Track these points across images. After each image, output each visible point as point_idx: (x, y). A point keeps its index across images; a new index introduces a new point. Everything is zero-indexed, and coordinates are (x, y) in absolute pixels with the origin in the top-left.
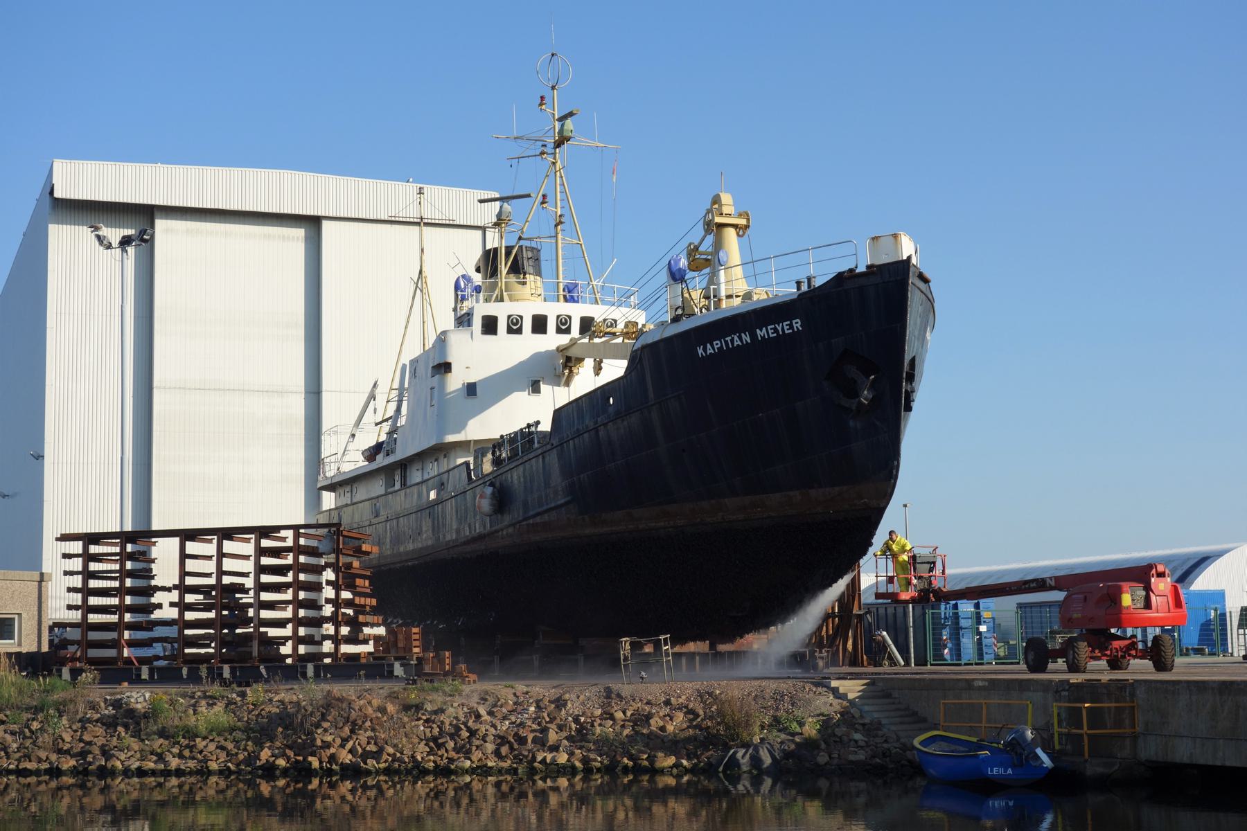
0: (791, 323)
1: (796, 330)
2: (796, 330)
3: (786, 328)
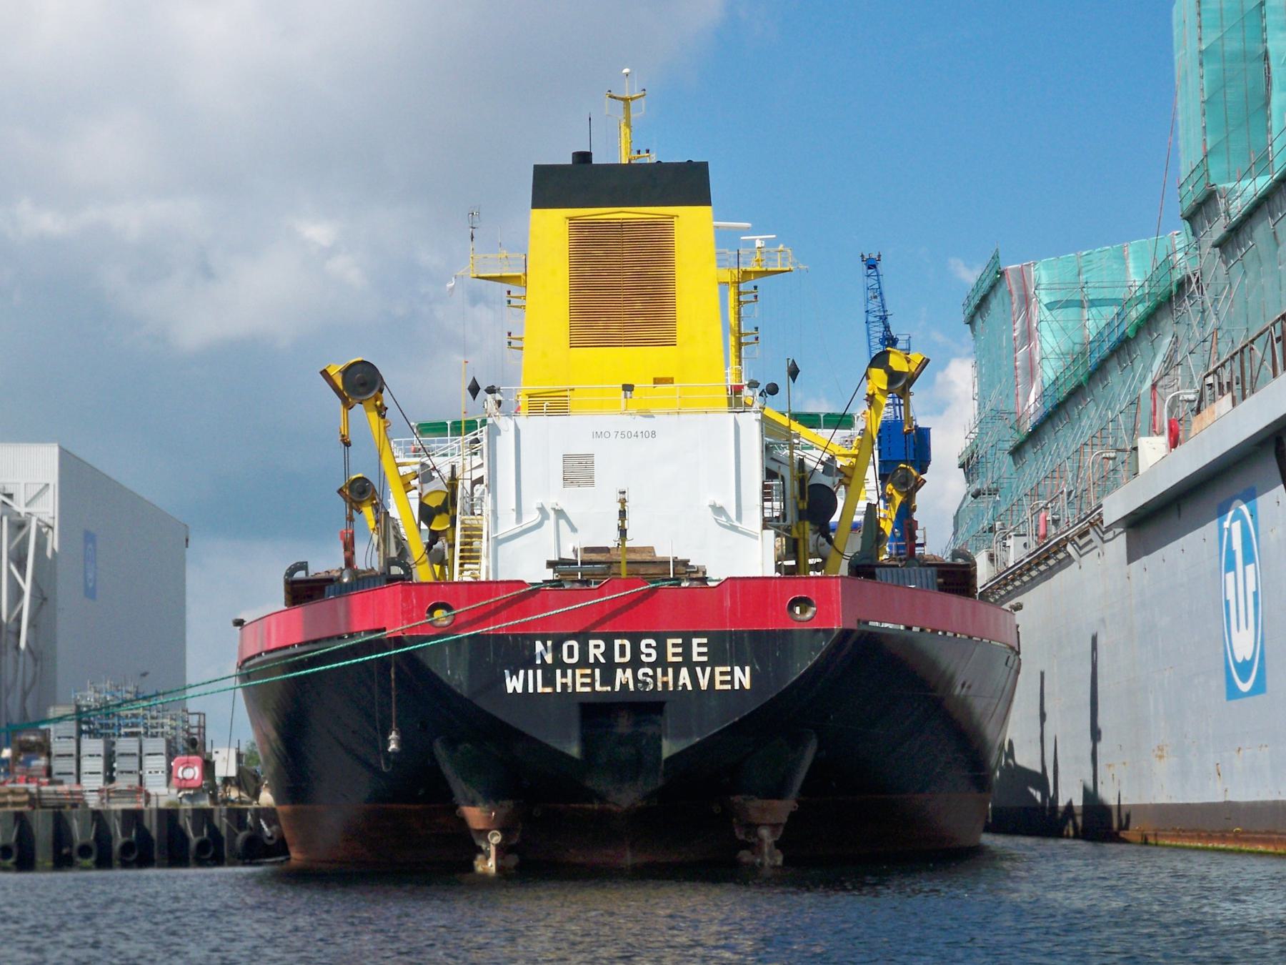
0: (731, 673)
1: (737, 687)
2: (737, 687)
3: (718, 678)
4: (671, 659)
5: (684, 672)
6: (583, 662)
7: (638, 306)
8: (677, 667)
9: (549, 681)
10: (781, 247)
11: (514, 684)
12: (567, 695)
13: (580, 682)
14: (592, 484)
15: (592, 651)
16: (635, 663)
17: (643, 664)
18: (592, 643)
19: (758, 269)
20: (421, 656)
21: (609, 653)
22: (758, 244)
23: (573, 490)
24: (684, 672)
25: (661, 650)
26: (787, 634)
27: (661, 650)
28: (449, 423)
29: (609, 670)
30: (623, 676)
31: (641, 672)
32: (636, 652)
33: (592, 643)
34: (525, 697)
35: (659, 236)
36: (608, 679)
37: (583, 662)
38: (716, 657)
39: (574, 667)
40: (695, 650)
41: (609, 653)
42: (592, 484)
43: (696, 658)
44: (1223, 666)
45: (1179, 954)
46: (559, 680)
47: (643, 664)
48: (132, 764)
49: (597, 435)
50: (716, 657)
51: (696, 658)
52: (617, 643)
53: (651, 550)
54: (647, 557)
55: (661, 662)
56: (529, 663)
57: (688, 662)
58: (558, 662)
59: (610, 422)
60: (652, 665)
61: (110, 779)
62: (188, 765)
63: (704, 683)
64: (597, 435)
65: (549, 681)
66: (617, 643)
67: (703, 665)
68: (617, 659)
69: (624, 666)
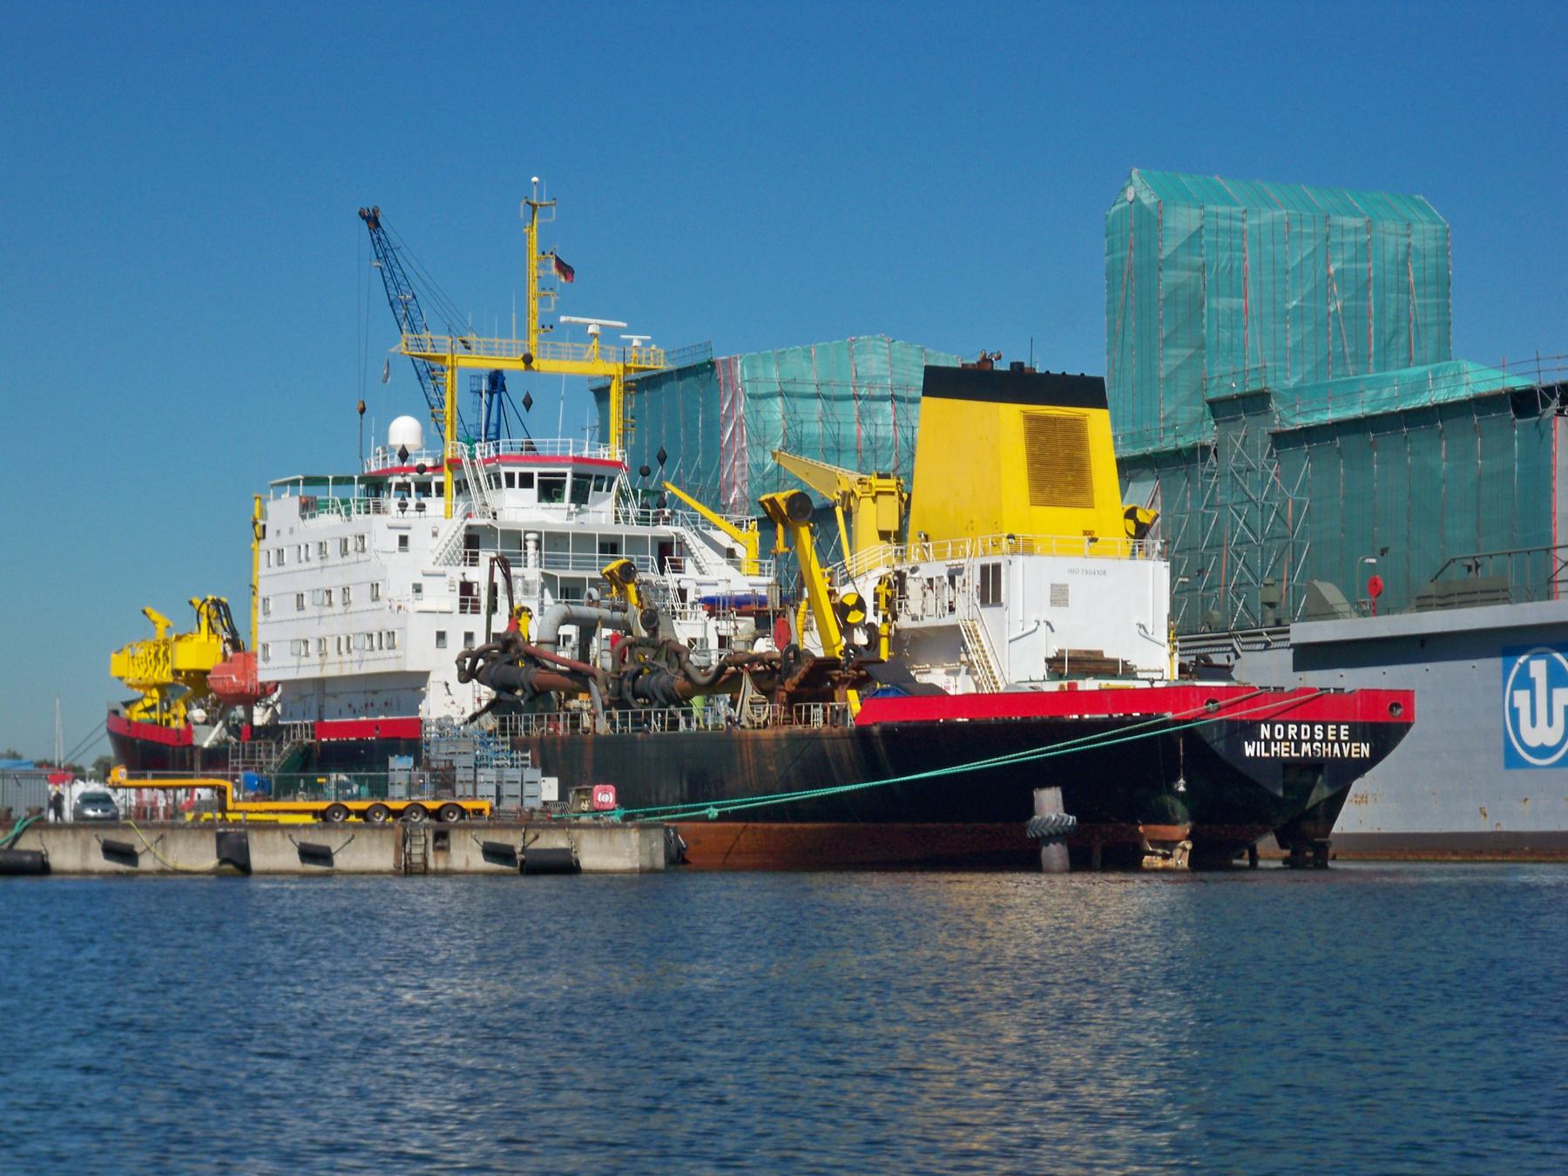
3: (1353, 750)
4: (1330, 738)
5: (1336, 745)
6: (1285, 739)
7: (1069, 479)
8: (1333, 743)
9: (1268, 749)
10: (653, 347)
11: (1249, 751)
12: (1277, 759)
13: (1282, 750)
14: (1067, 605)
15: (1290, 732)
16: (1312, 740)
17: (1316, 741)
18: (1290, 726)
19: (638, 366)
20: (1201, 731)
21: (1298, 734)
22: (636, 343)
23: (1056, 609)
24: (1336, 745)
25: (1325, 732)
26: (1388, 724)
27: (1325, 732)
28: (330, 477)
29: (1298, 743)
30: (1306, 747)
31: (1315, 745)
32: (1313, 733)
33: (1290, 726)
34: (1256, 759)
35: (1076, 431)
36: (1298, 750)
37: (1285, 739)
38: (1353, 738)
39: (1281, 741)
40: (1342, 732)
41: (1298, 734)
42: (1067, 605)
43: (1342, 738)
44: (1501, 744)
45: (1517, 917)
46: (1273, 749)
47: (1316, 741)
48: (515, 789)
49: (1072, 571)
50: (1353, 738)
51: (1342, 738)
52: (1303, 727)
53: (1101, 653)
54: (1098, 658)
55: (1325, 740)
56: (1258, 739)
57: (1339, 741)
58: (1272, 737)
59: (1076, 562)
60: (1321, 742)
61: (498, 803)
62: (605, 792)
63: (1346, 754)
64: (1072, 571)
65: (1268, 749)
66: (1303, 727)
67: (1346, 742)
68: (1303, 737)
69: (1306, 741)
